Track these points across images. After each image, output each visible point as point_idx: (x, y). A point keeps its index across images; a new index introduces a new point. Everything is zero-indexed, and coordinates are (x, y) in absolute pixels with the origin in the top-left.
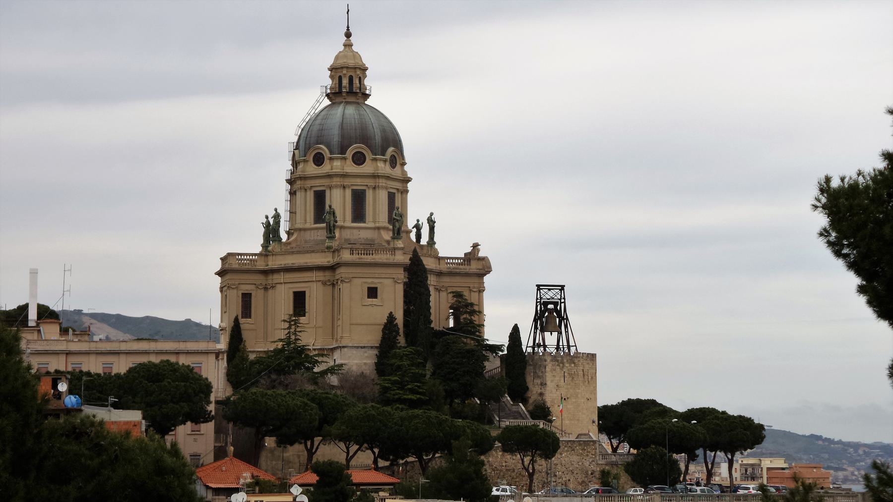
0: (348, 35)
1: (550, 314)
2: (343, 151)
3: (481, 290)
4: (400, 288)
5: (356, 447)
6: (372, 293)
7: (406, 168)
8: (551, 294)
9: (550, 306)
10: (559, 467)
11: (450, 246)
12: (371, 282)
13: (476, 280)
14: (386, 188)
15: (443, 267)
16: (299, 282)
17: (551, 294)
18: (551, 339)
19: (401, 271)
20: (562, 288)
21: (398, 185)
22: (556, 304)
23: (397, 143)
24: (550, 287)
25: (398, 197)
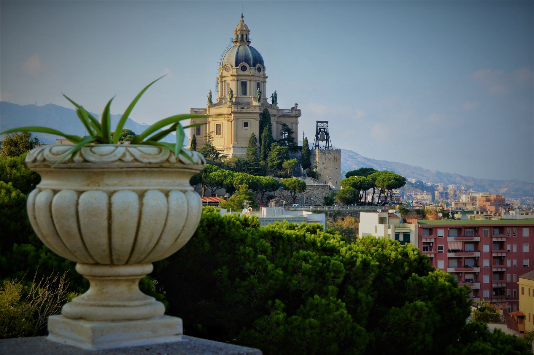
0: (242, 17)
1: (322, 133)
2: (254, 66)
3: (297, 124)
4: (257, 123)
5: (215, 188)
6: (246, 125)
7: (265, 72)
8: (322, 125)
9: (322, 130)
10: (312, 196)
11: (283, 105)
12: (246, 120)
13: (295, 119)
14: (256, 81)
15: (281, 114)
16: (218, 121)
17: (322, 125)
18: (322, 143)
19: (258, 115)
20: (327, 122)
21: (262, 79)
22: (324, 129)
23: (261, 62)
24: (322, 122)
25: (262, 85)
